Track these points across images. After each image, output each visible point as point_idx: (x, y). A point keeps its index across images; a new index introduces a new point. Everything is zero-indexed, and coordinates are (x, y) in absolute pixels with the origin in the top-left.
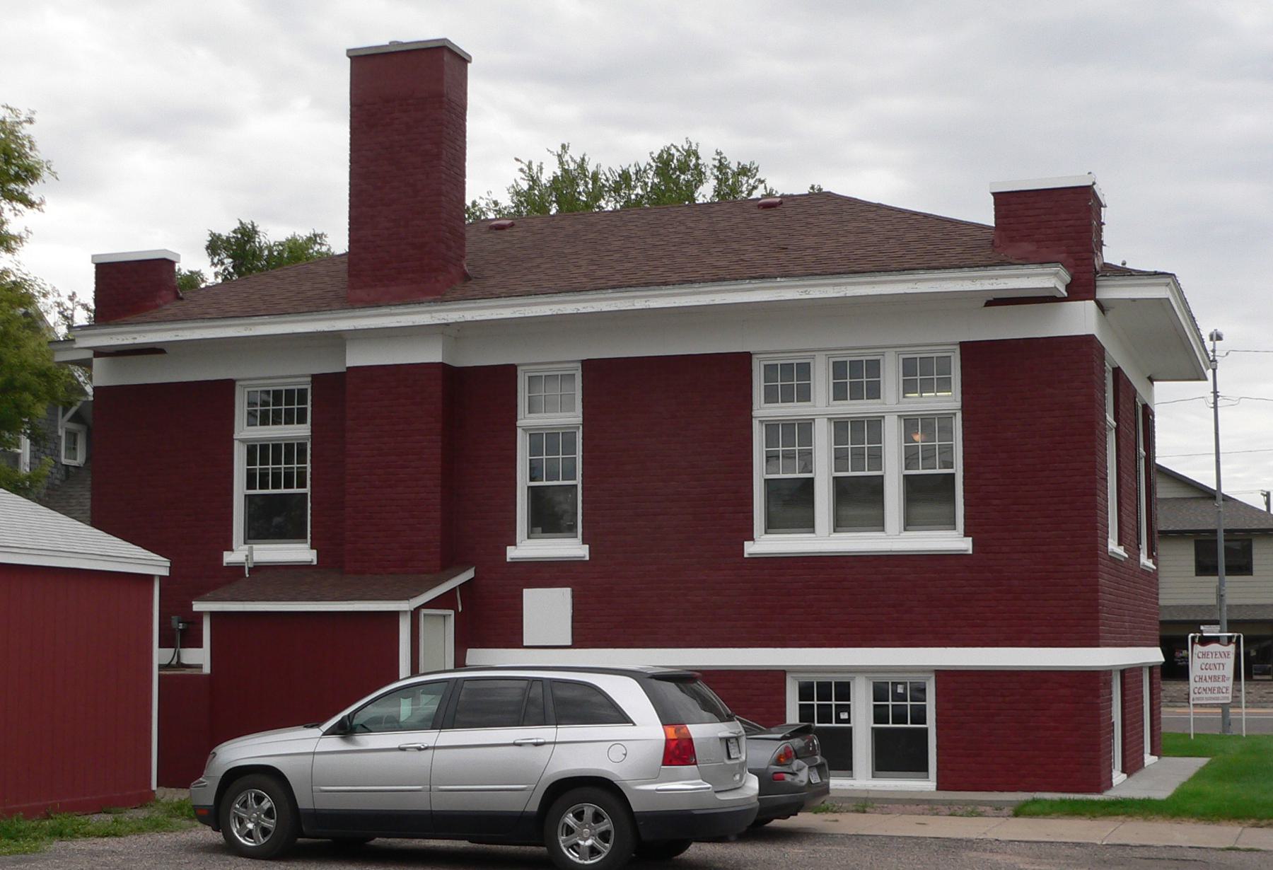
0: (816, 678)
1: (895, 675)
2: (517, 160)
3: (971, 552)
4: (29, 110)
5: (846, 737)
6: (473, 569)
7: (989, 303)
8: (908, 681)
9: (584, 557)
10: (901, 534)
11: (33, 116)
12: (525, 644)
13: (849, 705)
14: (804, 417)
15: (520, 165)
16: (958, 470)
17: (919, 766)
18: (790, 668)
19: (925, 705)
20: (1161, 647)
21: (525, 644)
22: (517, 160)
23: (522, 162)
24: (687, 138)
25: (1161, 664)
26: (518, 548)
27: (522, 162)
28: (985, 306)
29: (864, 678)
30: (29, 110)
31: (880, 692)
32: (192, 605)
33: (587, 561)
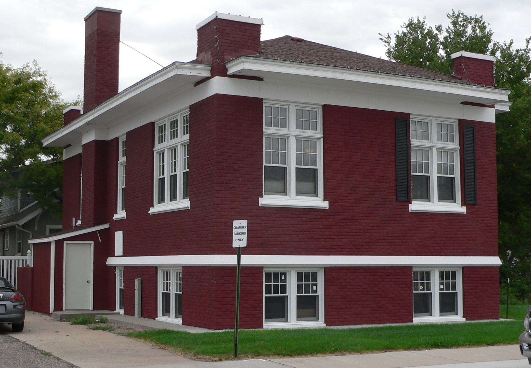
0: (304, 271)
1: (273, 269)
2: (379, 34)
3: (465, 213)
4: (27, 62)
5: (284, 301)
6: (109, 224)
7: (463, 103)
8: (419, 271)
9: (464, 212)
10: (181, 201)
11: (28, 65)
12: (115, 255)
13: (317, 284)
14: (161, 150)
15: (380, 36)
16: (320, 167)
17: (315, 316)
18: (159, 265)
19: (286, 284)
20: (499, 257)
21: (115, 255)
22: (379, 34)
23: (381, 35)
24: (452, 9)
25: (499, 266)
26: (118, 214)
27: (381, 35)
28: (195, 86)
29: (438, 270)
30: (27, 62)
31: (300, 277)
32: (28, 241)
33: (465, 214)
